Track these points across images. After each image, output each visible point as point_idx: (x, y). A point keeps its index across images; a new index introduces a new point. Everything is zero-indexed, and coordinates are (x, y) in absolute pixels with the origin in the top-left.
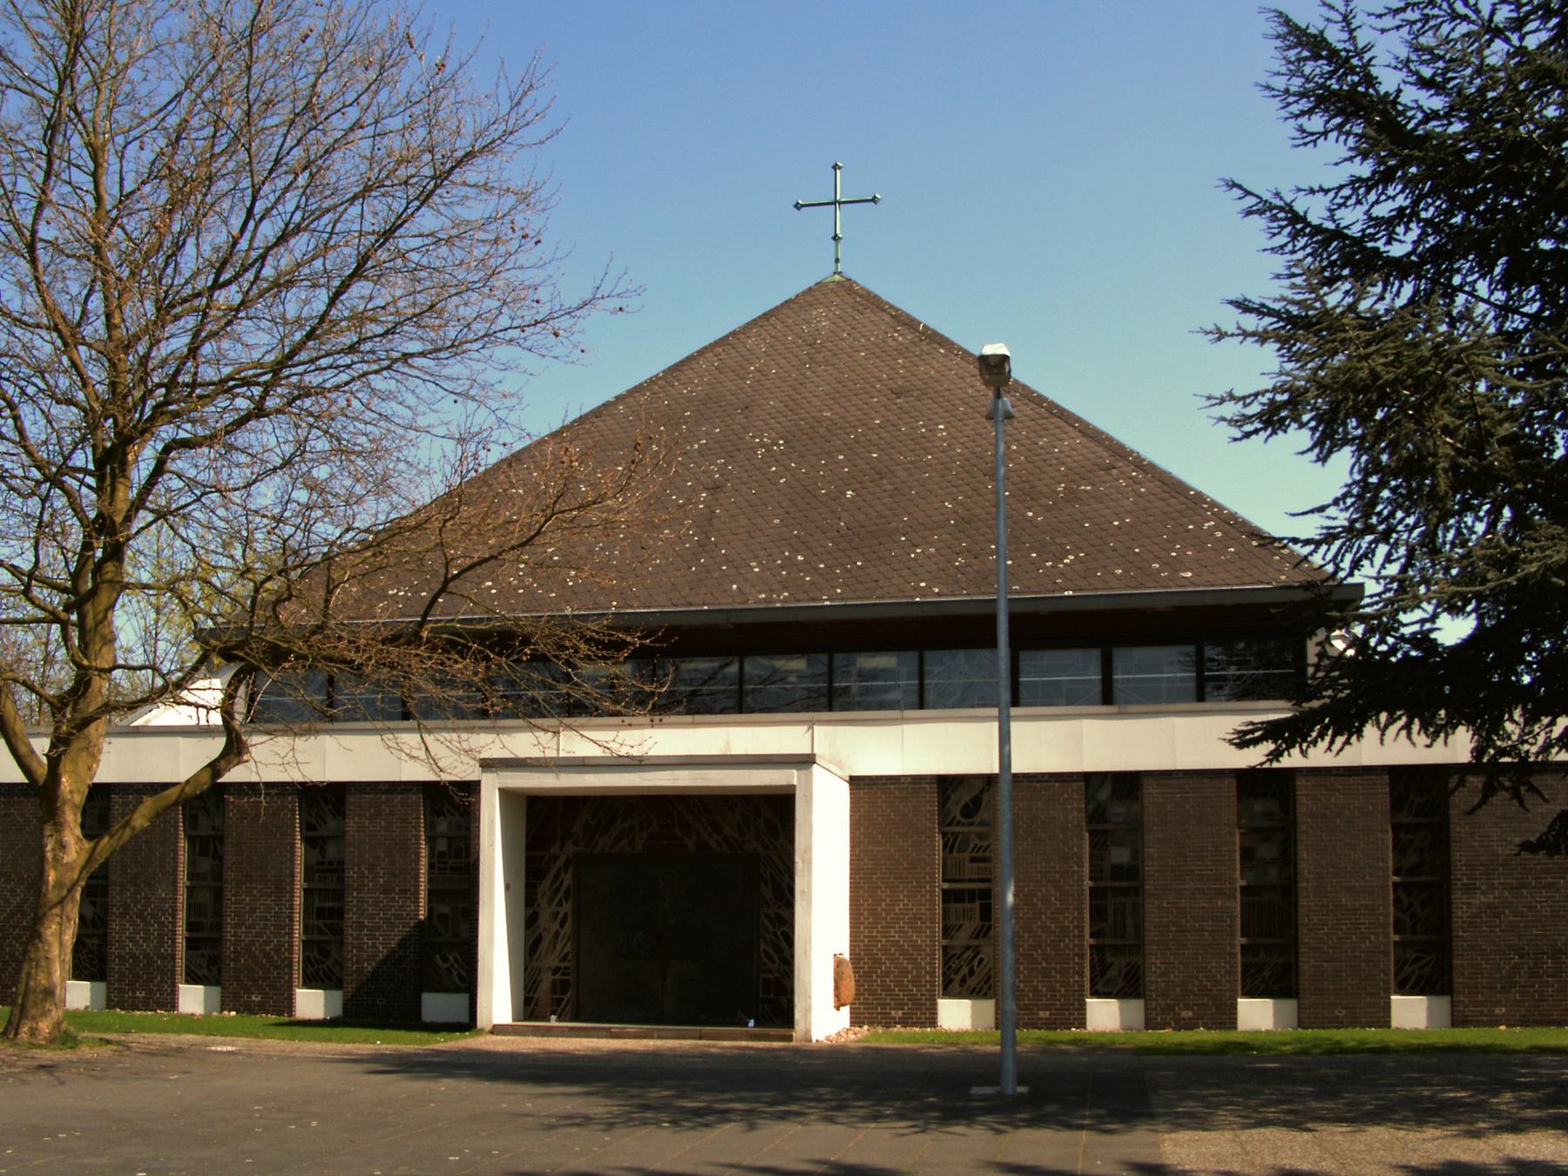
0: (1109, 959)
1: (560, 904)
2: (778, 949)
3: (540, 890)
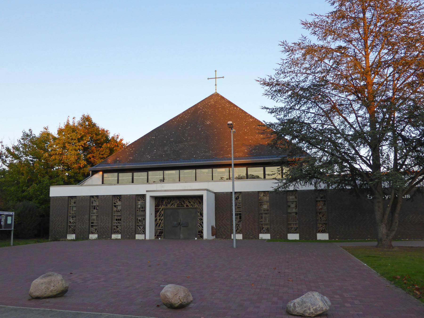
2: (201, 225)
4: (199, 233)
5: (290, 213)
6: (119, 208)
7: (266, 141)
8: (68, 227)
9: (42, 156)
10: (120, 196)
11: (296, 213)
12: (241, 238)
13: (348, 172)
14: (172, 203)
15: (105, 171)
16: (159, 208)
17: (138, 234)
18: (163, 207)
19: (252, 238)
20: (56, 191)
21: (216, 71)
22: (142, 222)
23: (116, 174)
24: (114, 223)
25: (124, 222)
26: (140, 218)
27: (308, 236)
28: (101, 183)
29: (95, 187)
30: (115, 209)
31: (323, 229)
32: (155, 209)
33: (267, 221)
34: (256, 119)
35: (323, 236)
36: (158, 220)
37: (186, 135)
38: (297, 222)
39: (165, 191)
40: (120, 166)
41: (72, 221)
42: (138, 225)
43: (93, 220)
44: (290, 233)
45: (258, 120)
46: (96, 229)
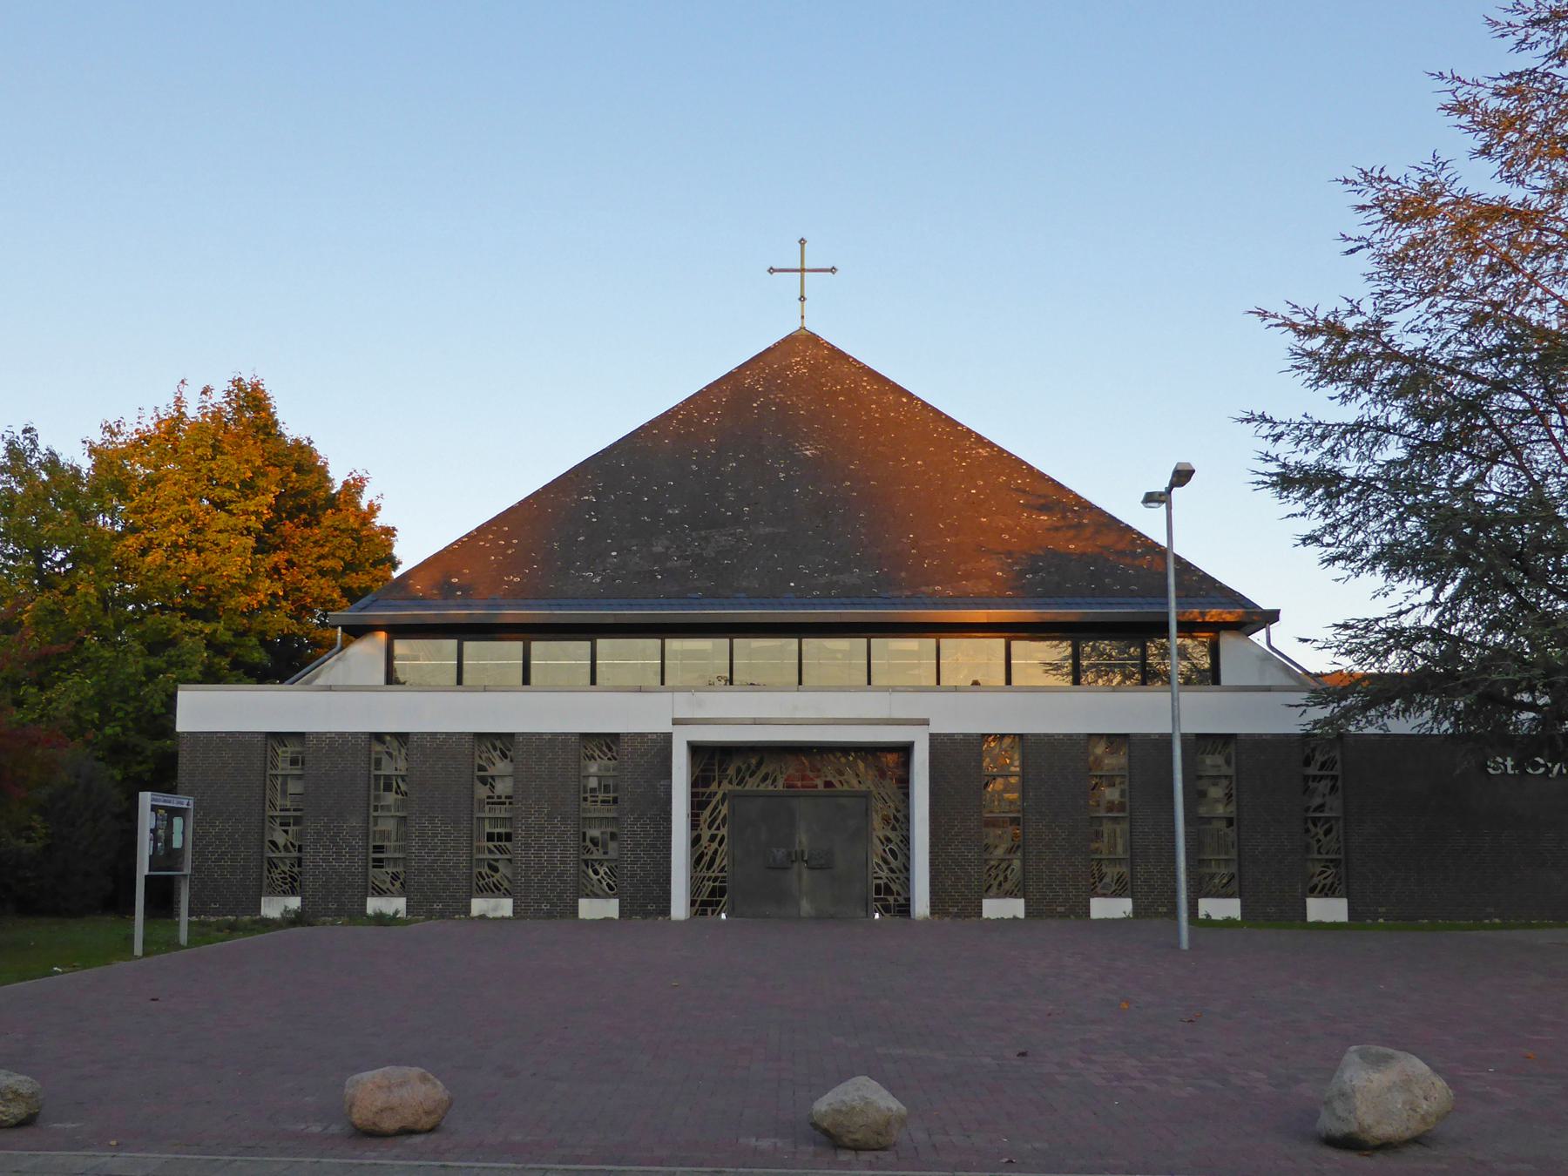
0: (1104, 869)
1: (718, 828)
3: (702, 819)
4: (878, 891)
5: (1209, 820)
6: (503, 788)
7: (1070, 541)
8: (266, 866)
9: (108, 551)
10: (615, 737)
11: (1230, 822)
12: (1021, 915)
13: (1085, 663)
14: (763, 770)
15: (398, 631)
16: (708, 791)
17: (588, 896)
18: (726, 787)
19: (1063, 916)
20: (204, 710)
21: (802, 242)
22: (605, 846)
23: (451, 644)
24: (480, 850)
25: (527, 846)
26: (595, 832)
27: (1273, 907)
28: (380, 678)
29: (350, 697)
30: (482, 792)
31: (1329, 881)
32: (693, 795)
33: (1120, 849)
34: (1001, 450)
35: (1327, 910)
36: (704, 841)
37: (731, 496)
38: (1233, 854)
39: (756, 722)
40: (477, 613)
41: (281, 839)
42: (586, 862)
43: (384, 835)
44: (1206, 896)
45: (1010, 455)
46: (395, 877)
